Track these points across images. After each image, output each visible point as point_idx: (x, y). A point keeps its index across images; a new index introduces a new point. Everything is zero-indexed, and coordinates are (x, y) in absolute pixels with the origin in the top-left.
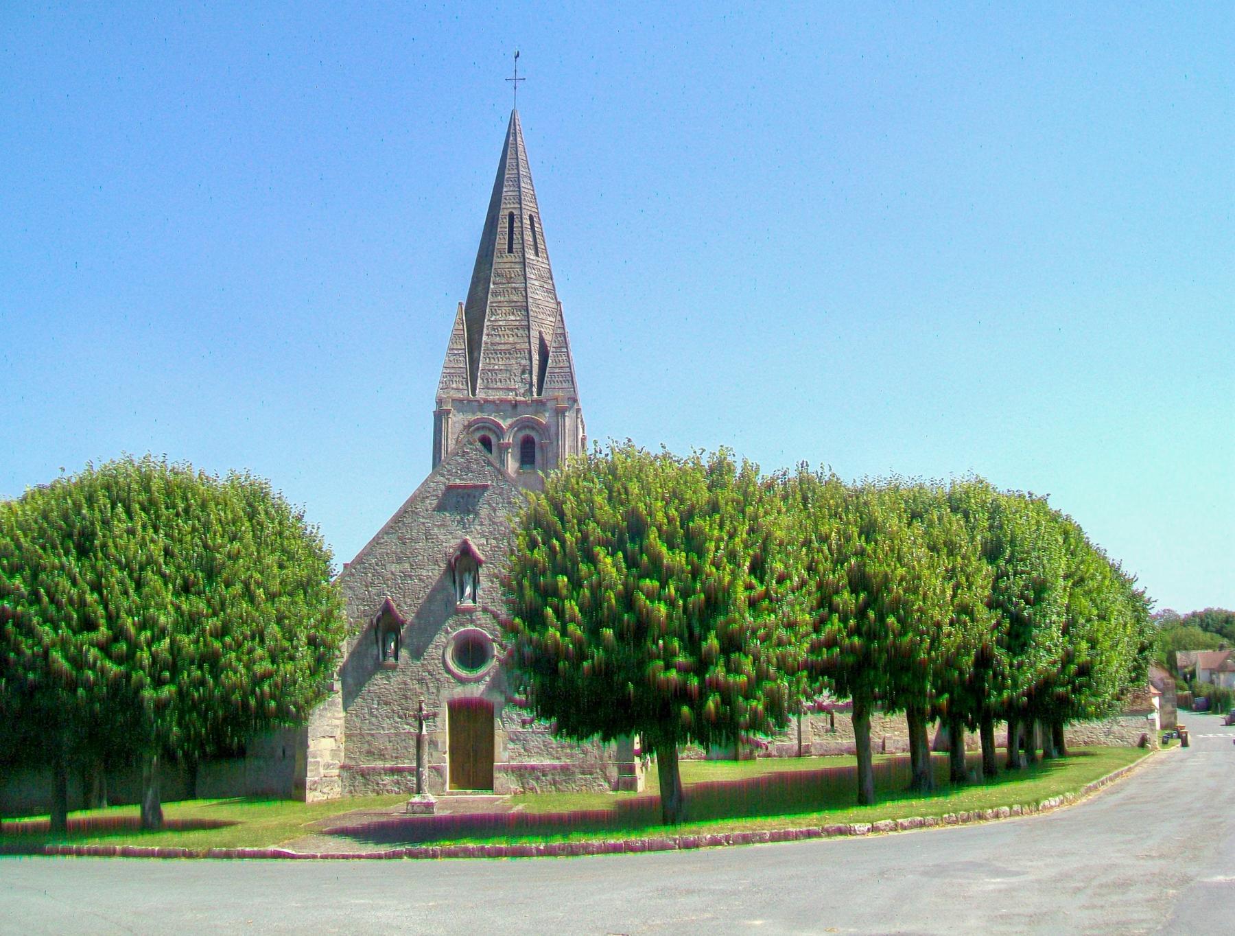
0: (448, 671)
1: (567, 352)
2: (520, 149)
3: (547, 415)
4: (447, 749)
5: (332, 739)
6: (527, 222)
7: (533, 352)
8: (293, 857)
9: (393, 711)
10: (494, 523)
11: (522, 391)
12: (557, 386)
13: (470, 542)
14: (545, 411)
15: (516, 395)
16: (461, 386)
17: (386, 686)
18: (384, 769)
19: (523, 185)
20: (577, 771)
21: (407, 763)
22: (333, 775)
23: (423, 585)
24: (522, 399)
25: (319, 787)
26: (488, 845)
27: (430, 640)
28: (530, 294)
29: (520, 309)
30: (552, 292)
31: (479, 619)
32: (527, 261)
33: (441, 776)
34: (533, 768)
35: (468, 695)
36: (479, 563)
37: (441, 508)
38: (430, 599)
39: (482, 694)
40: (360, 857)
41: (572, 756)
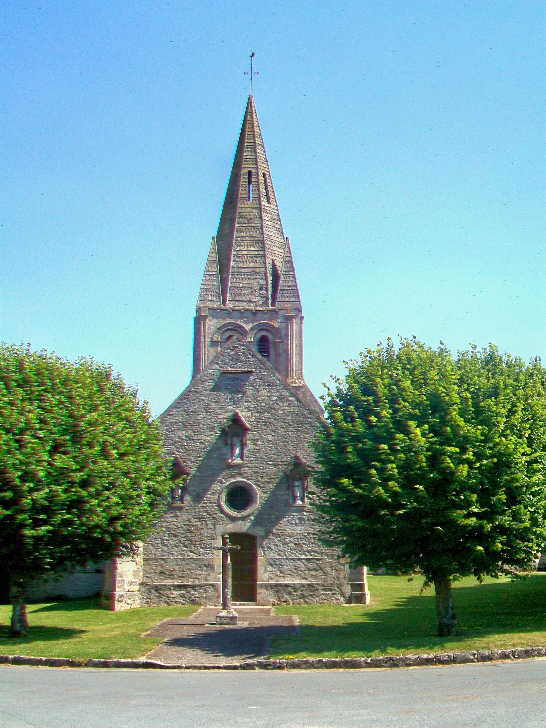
0: (222, 511)
1: (294, 275)
2: (256, 124)
3: (279, 321)
4: (221, 571)
5: (134, 563)
6: (261, 178)
7: (269, 275)
8: (161, 667)
9: (180, 541)
10: (258, 401)
11: (260, 303)
12: (287, 299)
13: (240, 414)
14: (278, 318)
15: (257, 306)
16: (215, 299)
17: (175, 523)
18: (174, 586)
19: (258, 151)
20: (320, 588)
21: (191, 582)
22: (135, 590)
23: (203, 446)
24: (261, 309)
25: (125, 599)
26: (325, 658)
27: (207, 490)
28: (265, 232)
29: (258, 242)
30: (280, 230)
31: (246, 473)
32: (263, 207)
33: (217, 592)
34: (287, 586)
35: (238, 531)
36: (246, 429)
37: (216, 388)
38: (208, 457)
39: (248, 529)
40: (219, 668)
41: (316, 577)
